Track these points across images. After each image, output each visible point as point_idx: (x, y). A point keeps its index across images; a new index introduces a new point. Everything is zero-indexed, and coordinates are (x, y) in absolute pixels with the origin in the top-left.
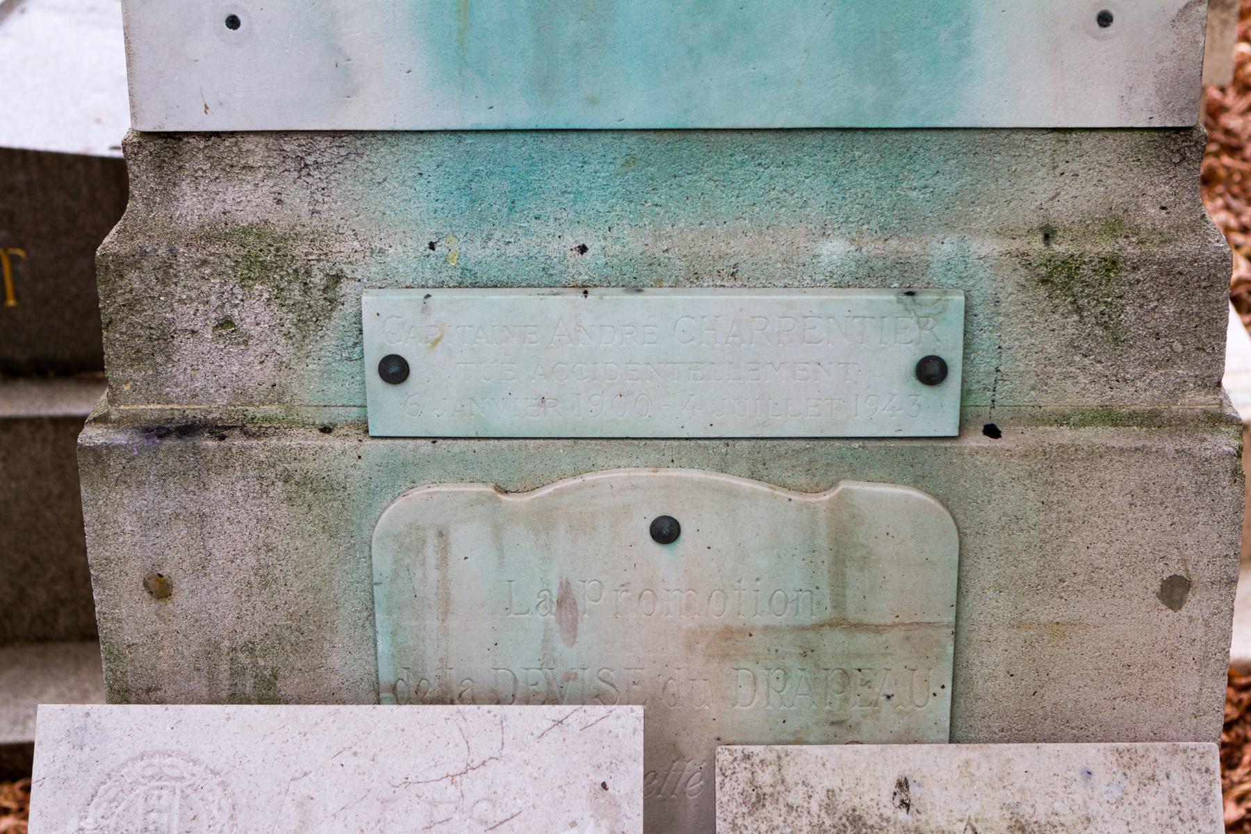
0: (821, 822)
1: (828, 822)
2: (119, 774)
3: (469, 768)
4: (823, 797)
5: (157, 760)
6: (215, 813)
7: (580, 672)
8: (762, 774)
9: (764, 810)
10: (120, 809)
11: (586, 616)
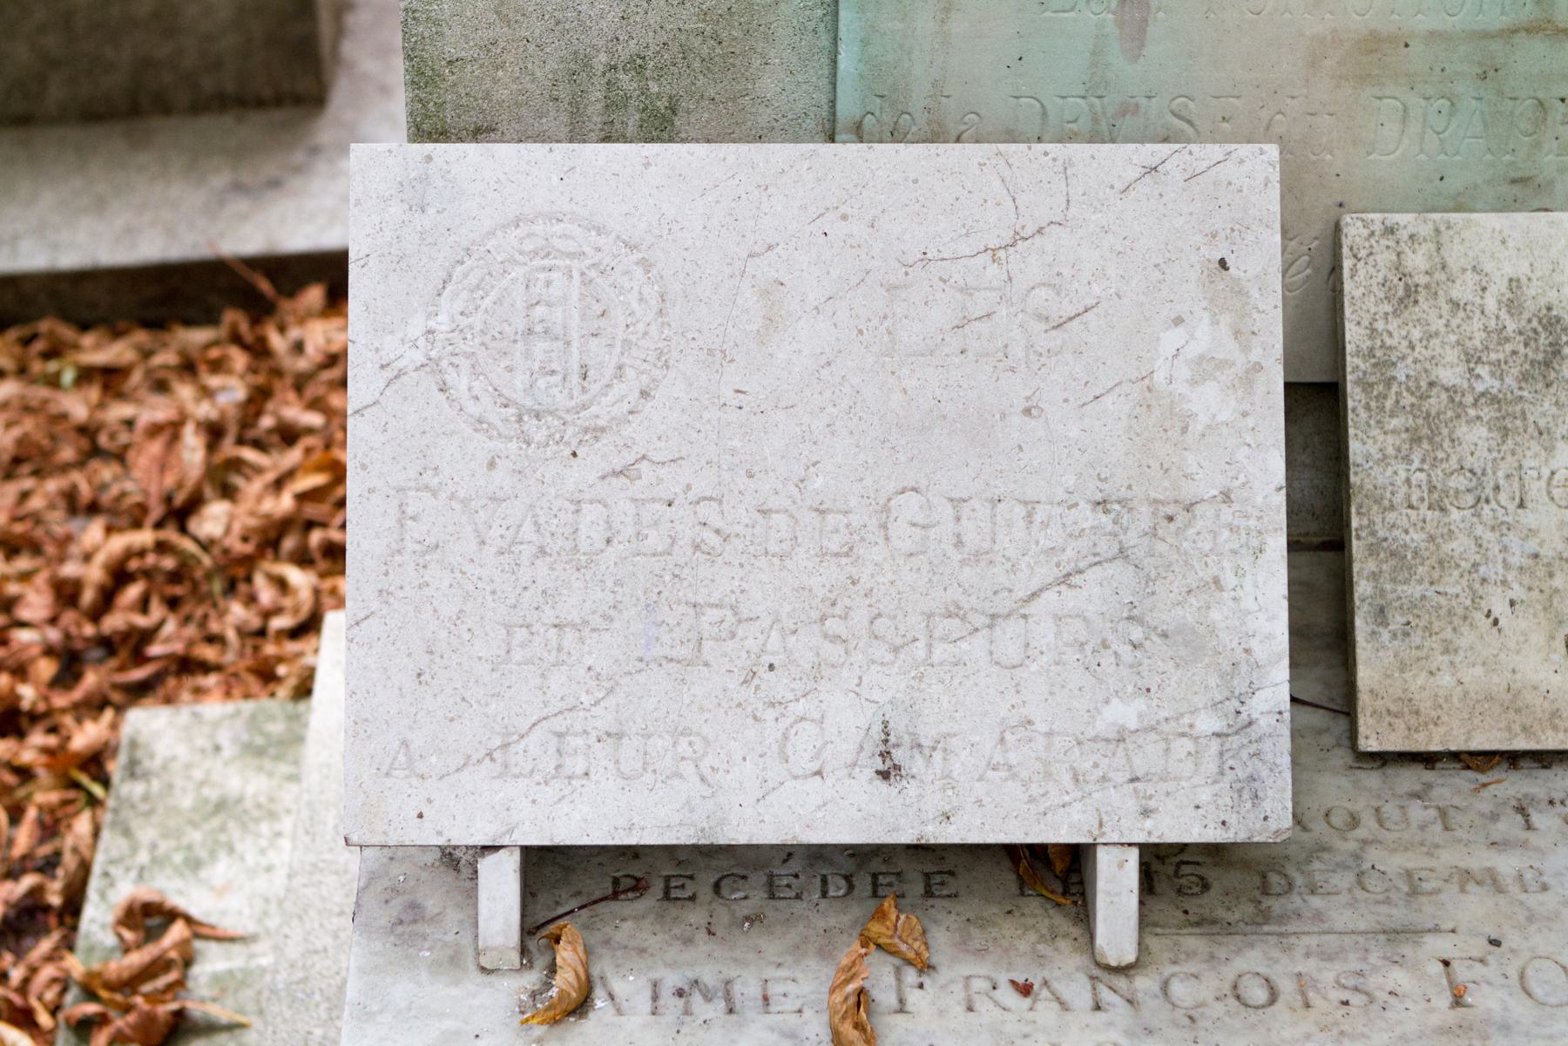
0: (1500, 326)
1: (1511, 326)
2: (482, 249)
3: (1018, 238)
4: (1504, 289)
5: (541, 227)
6: (635, 306)
7: (1144, 101)
8: (1413, 256)
9: (1417, 309)
10: (488, 301)
11: (1161, 15)
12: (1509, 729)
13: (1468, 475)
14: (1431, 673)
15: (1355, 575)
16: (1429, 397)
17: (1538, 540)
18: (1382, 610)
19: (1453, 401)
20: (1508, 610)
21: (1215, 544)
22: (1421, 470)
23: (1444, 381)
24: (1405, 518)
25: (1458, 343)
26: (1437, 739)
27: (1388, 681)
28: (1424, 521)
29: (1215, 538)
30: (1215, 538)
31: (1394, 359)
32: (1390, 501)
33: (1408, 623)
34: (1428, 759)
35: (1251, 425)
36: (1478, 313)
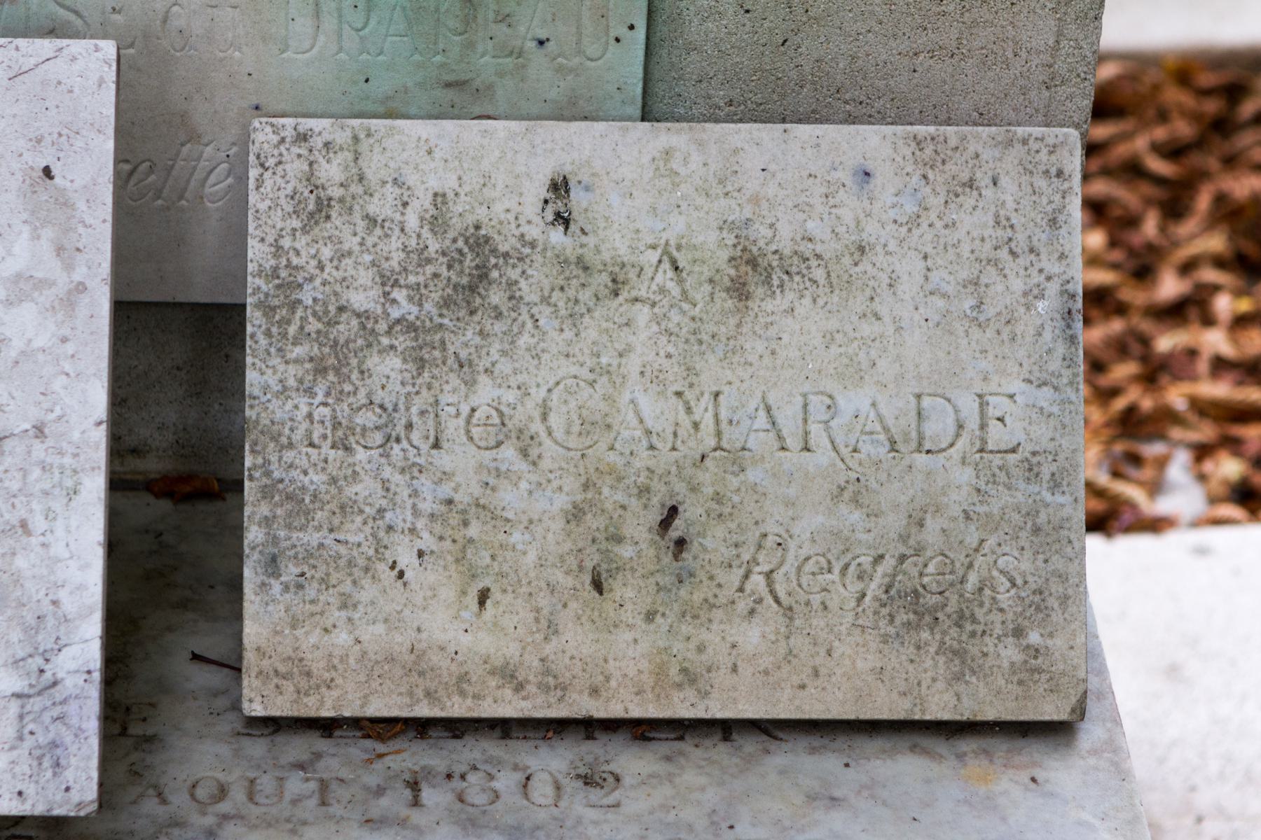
0: (422, 246)
1: (434, 246)
4: (427, 203)
8: (328, 166)
9: (328, 225)
12: (411, 694)
13: (378, 410)
14: (326, 630)
15: (246, 519)
16: (338, 323)
17: (453, 485)
18: (274, 559)
19: (364, 328)
20: (416, 561)
21: (25, 483)
22: (325, 404)
23: (356, 306)
24: (304, 457)
25: (373, 264)
26: (329, 703)
27: (278, 638)
28: (326, 461)
29: (25, 477)
30: (25, 477)
31: (300, 280)
32: (289, 438)
33: (303, 574)
34: (327, 727)
35: (70, 352)
36: (397, 231)
